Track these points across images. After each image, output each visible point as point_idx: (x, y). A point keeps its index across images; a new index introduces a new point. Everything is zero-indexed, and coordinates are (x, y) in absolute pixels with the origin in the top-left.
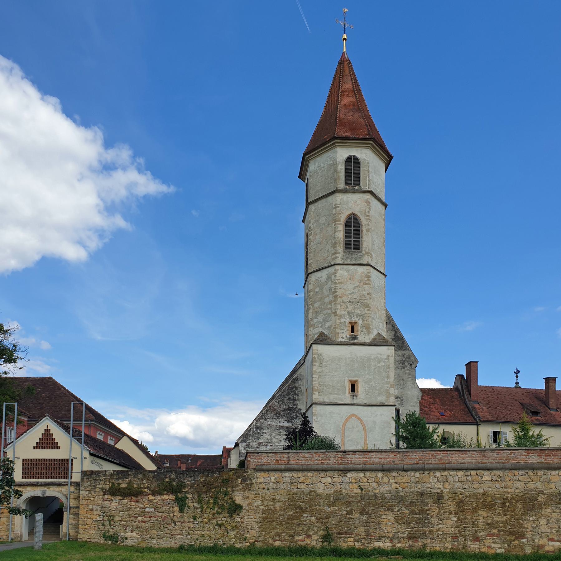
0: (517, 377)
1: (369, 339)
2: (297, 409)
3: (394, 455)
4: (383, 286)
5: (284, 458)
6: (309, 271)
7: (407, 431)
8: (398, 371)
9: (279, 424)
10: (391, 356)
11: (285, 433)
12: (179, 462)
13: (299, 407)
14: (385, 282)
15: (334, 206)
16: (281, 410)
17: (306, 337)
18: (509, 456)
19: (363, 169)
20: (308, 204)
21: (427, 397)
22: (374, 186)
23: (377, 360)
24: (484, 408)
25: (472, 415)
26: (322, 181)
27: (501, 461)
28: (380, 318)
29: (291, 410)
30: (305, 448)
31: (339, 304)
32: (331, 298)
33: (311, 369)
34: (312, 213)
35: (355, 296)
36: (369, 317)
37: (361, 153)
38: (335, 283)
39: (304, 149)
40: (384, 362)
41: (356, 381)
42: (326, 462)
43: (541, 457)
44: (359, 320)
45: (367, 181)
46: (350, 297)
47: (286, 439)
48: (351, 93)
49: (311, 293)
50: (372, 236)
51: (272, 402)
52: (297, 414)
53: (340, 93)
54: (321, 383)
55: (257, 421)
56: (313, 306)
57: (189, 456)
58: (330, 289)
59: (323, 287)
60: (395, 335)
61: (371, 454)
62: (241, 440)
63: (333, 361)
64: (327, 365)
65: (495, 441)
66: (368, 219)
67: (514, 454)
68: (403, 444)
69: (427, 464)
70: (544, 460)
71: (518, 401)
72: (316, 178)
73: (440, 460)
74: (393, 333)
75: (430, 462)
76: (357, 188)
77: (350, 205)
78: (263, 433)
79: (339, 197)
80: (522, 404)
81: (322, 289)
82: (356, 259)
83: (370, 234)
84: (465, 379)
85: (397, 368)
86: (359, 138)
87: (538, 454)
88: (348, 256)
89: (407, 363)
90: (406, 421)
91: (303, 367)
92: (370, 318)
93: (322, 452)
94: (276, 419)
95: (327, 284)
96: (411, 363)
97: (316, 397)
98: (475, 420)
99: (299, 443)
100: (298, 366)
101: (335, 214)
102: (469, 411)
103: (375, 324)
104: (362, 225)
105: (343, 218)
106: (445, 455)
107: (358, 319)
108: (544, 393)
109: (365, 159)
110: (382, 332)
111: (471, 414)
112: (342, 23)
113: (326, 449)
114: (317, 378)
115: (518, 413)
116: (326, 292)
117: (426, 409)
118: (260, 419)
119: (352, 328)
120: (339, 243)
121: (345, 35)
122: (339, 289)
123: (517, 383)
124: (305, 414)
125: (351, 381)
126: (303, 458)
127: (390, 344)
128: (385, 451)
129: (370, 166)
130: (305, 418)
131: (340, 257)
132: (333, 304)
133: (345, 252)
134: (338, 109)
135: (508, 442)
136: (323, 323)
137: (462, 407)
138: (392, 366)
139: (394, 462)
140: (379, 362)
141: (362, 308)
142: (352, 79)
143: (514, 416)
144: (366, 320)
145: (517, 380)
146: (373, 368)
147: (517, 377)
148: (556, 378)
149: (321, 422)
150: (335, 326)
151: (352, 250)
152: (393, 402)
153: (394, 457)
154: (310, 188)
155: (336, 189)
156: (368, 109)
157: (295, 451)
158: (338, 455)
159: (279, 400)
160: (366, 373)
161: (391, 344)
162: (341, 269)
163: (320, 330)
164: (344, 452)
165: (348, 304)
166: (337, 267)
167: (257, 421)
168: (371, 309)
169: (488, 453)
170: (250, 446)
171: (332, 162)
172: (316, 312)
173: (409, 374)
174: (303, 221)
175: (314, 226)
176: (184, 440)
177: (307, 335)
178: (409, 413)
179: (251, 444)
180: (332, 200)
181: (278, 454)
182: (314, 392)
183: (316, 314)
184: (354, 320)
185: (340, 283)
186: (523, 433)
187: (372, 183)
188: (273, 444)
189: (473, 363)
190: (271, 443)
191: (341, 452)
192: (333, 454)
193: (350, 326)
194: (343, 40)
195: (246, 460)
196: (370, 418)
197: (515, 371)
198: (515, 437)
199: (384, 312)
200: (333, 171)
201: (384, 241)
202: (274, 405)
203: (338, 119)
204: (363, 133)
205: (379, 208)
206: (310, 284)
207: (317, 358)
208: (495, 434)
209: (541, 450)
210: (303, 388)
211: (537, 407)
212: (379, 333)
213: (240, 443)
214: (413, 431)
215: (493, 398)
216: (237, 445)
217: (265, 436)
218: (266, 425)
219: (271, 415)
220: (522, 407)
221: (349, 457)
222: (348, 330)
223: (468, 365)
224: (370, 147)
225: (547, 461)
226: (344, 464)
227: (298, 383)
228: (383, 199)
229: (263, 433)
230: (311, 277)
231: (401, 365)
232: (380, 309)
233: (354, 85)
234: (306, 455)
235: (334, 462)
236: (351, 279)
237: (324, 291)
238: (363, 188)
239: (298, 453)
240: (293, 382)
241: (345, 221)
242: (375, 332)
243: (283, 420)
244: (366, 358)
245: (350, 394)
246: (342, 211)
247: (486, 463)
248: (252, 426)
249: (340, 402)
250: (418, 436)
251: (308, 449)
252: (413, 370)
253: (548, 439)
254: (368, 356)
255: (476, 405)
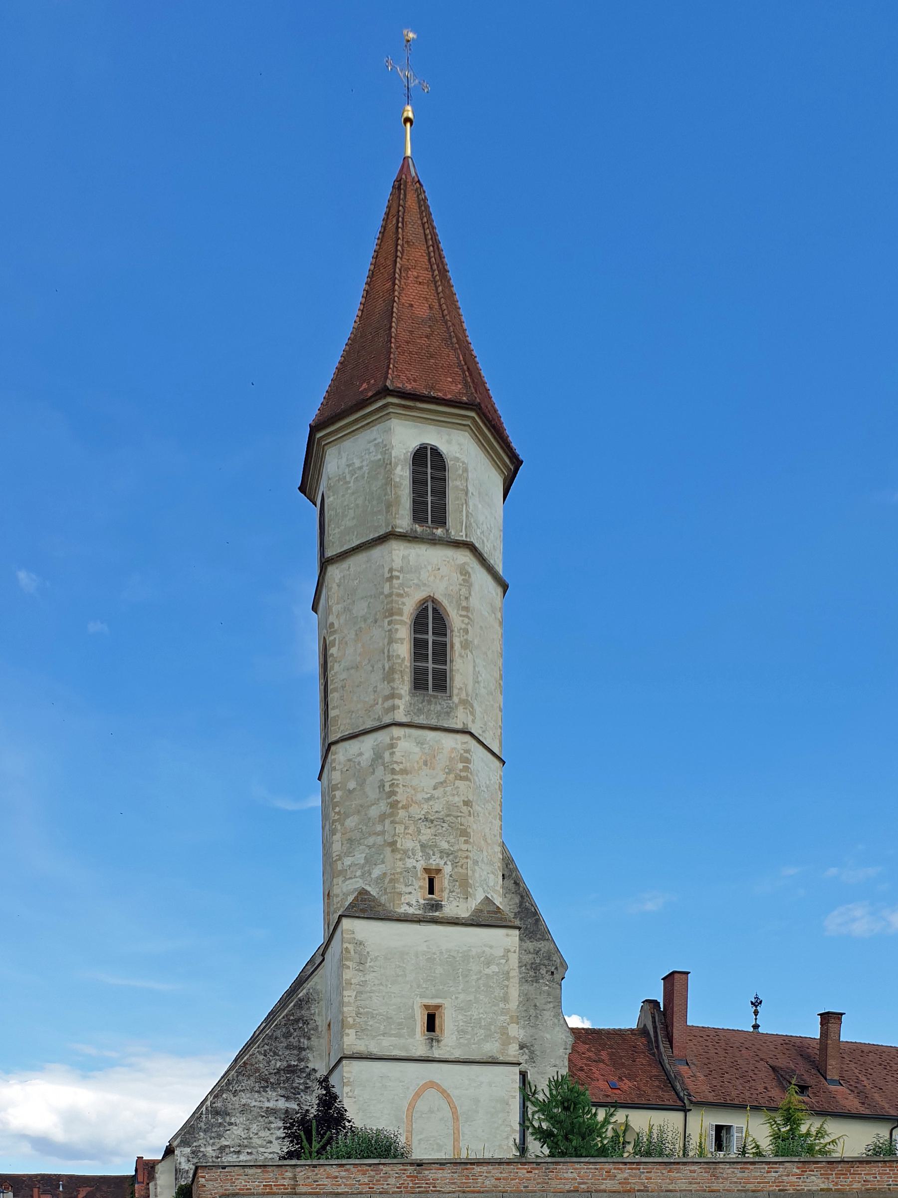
0: (756, 1013)
1: (468, 910)
2: (308, 1070)
3: (528, 1172)
4: (497, 787)
5: (284, 1178)
6: (333, 738)
7: (552, 1118)
8: (526, 987)
9: (267, 1104)
10: (512, 950)
11: (280, 1124)
12: (36, 1190)
13: (311, 1066)
14: (501, 778)
15: (387, 575)
16: (272, 1071)
17: (326, 901)
18: (765, 1175)
19: (453, 485)
20: (325, 563)
21: (582, 1048)
22: (479, 533)
23: (482, 959)
24: (698, 1074)
25: (675, 1089)
26: (357, 505)
27: (749, 1186)
28: (491, 863)
29: (293, 1072)
30: (332, 1156)
31: (401, 823)
32: (383, 807)
33: (340, 976)
34: (335, 586)
35: (436, 805)
36: (467, 858)
37: (449, 442)
38: (393, 771)
39: (311, 415)
40: (498, 964)
41: (438, 1007)
42: (378, 1187)
43: (828, 1178)
44: (445, 863)
45: (462, 516)
46: (425, 807)
47: (284, 1138)
48: (426, 275)
49: (338, 794)
50: (474, 661)
51: (250, 1053)
52: (308, 1081)
53: (397, 270)
54: (362, 1010)
55: (216, 1097)
56: (342, 825)
57: (59, 1177)
58: (382, 786)
59: (365, 780)
60: (521, 903)
61: (477, 1169)
62: (178, 1140)
63: (389, 959)
64: (376, 969)
65: (719, 1147)
66: (464, 616)
67: (776, 1172)
68: (542, 1147)
69: (596, 1191)
70: (834, 1185)
71: (767, 1062)
72: (343, 496)
73: (625, 1183)
74: (517, 900)
75: (603, 1187)
76: (439, 532)
77: (424, 575)
78: (231, 1124)
79: (398, 552)
80: (773, 1068)
81: (362, 783)
82: (439, 715)
83: (469, 653)
84: (662, 1010)
85: (523, 980)
86: (444, 399)
87: (822, 1172)
88: (420, 705)
89: (545, 970)
90: (549, 1096)
91: (320, 971)
92: (469, 860)
93: (370, 1165)
94: (258, 1092)
95: (373, 773)
96: (553, 969)
97: (352, 1042)
98: (682, 1100)
99: (316, 1146)
100: (309, 970)
101: (391, 595)
102: (669, 1081)
103: (481, 876)
104: (452, 631)
105: (409, 608)
106: (634, 1171)
107: (442, 862)
108: (818, 1047)
109: (457, 459)
110: (495, 896)
111: (672, 1087)
112: (401, 70)
113: (379, 1156)
114: (353, 997)
115: (766, 1088)
116: (372, 793)
117: (579, 1073)
118: (222, 1091)
119: (431, 882)
120: (401, 672)
121: (409, 108)
122: (401, 786)
123: (756, 1027)
124: (326, 1079)
125: (427, 1007)
126: (327, 1178)
127: (510, 924)
128: (507, 1161)
129: (470, 480)
130: (327, 1088)
131: (402, 707)
132: (387, 822)
133: (413, 695)
134: (394, 315)
135: (757, 1147)
136: (366, 869)
137: (655, 1072)
138: (515, 973)
139: (527, 1187)
140: (488, 964)
141: (452, 837)
142: (426, 235)
143: (757, 1094)
144: (460, 864)
145: (756, 1019)
146: (475, 977)
147: (756, 1013)
148: (842, 1014)
149: (361, 1099)
150: (393, 877)
151: (430, 691)
152: (515, 1057)
153: (528, 1175)
154: (330, 521)
155: (390, 529)
156: (465, 326)
157: (309, 1162)
158: (405, 1170)
159: (266, 1047)
160: (460, 988)
161: (512, 924)
162: (405, 736)
163: (358, 884)
164: (420, 1164)
165: (422, 825)
166: (396, 732)
167: (215, 1097)
168: (471, 840)
169: (722, 1169)
170: (200, 1154)
171: (379, 457)
172: (350, 841)
173: (549, 994)
174: (315, 608)
175: (342, 621)
176: (42, 1144)
177: (328, 895)
178: (555, 1078)
179: (202, 1149)
180: (383, 557)
181: (270, 1169)
182: (347, 1031)
183: (348, 845)
184: (434, 863)
185: (404, 772)
186: (788, 1128)
187: (474, 524)
188: (254, 1151)
189: (678, 975)
190: (249, 1148)
191: (412, 1164)
192: (396, 1169)
193: (426, 876)
194: (405, 123)
195: (195, 1183)
196: (467, 1090)
197: (754, 1001)
198: (771, 1136)
199: (498, 849)
200: (384, 481)
201: (501, 676)
202: (254, 1061)
203: (393, 340)
204: (452, 388)
205: (488, 592)
206: (334, 769)
207: (352, 952)
208: (719, 1129)
209: (828, 1162)
210: (321, 1021)
211: (803, 1075)
212: (487, 898)
213: (178, 1146)
214: (563, 1117)
215: (716, 1053)
216: (169, 1151)
217: (235, 1132)
218: (237, 1106)
219: (249, 1082)
220: (773, 1076)
221: (431, 1175)
222: (420, 887)
223: (669, 979)
224: (471, 429)
225: (840, 1187)
226: (419, 1192)
227: (309, 1009)
228: (500, 569)
229: (231, 1124)
230: (336, 753)
231: (532, 973)
232: (489, 841)
233: (432, 254)
234: (334, 1171)
235: (398, 1188)
236: (429, 764)
237: (368, 789)
238: (455, 534)
239: (315, 1166)
240: (299, 1005)
241: (414, 616)
242: (480, 896)
243: (274, 1094)
244: (460, 955)
245: (424, 1035)
246: (406, 589)
247: (718, 1191)
248: (204, 1107)
249: (403, 1054)
250: (575, 1130)
251: (338, 1158)
252: (558, 986)
253: (837, 1141)
254: (465, 949)
255: (683, 1067)
